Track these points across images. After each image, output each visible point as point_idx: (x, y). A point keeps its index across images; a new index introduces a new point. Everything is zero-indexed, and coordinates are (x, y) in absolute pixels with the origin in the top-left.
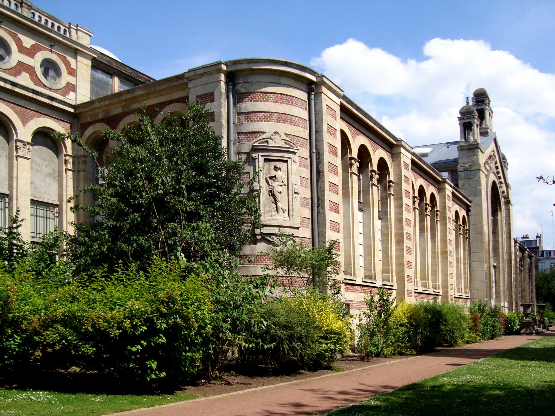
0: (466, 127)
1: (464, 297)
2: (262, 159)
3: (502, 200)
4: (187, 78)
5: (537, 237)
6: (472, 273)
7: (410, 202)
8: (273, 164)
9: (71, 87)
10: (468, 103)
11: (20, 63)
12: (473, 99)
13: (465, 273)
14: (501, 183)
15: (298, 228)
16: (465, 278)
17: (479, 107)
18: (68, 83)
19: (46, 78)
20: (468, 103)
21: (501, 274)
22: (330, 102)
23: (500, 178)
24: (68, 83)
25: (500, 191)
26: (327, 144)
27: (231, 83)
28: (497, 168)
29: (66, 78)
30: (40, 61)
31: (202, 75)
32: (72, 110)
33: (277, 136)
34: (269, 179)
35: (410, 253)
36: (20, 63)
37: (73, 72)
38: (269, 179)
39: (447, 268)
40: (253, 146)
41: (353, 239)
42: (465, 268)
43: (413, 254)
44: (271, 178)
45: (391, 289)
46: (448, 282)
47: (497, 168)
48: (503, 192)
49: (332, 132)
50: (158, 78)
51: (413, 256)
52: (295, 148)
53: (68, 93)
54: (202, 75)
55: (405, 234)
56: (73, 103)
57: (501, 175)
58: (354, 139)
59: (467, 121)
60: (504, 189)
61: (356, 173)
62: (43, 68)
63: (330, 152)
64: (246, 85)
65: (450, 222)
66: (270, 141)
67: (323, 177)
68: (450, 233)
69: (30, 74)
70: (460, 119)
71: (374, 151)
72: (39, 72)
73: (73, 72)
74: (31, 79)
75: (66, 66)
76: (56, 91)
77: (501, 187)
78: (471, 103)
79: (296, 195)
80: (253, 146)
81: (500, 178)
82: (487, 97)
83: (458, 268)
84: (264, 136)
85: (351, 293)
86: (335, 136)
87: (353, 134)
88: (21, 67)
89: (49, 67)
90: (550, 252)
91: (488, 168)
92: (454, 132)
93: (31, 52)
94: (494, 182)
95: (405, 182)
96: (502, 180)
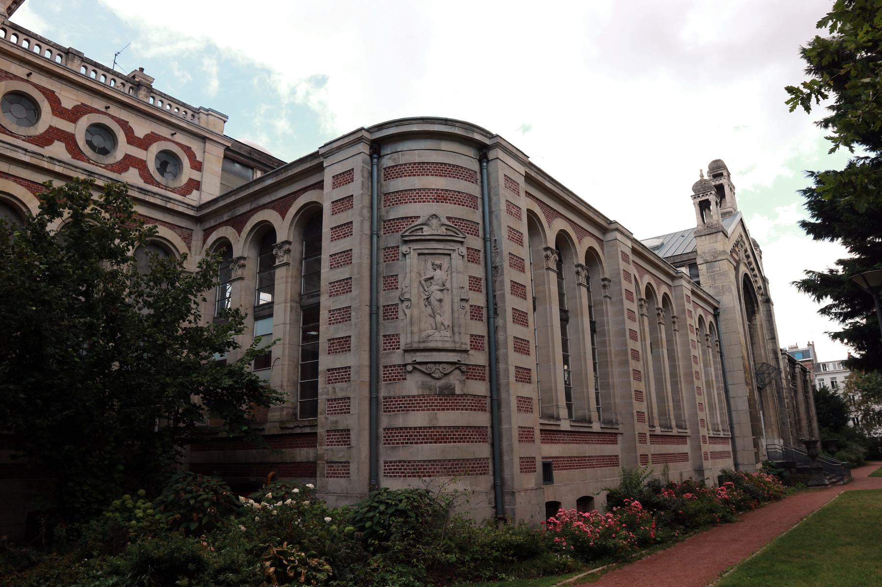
0: (704, 206)
1: (722, 436)
2: (414, 254)
3: (759, 298)
4: (322, 155)
5: (809, 345)
6: (732, 401)
7: (634, 307)
8: (430, 259)
9: (195, 185)
10: (702, 176)
11: (127, 157)
12: (708, 172)
13: (720, 401)
14: (755, 276)
15: (466, 351)
16: (721, 409)
17: (717, 183)
18: (190, 180)
19: (163, 175)
20: (702, 176)
21: (770, 399)
22: (502, 168)
23: (753, 270)
24: (190, 180)
25: (755, 286)
26: (507, 228)
27: (375, 156)
28: (748, 257)
29: (188, 173)
30: (156, 153)
31: (340, 148)
32: (192, 213)
33: (434, 221)
34: (423, 282)
35: (639, 379)
36: (127, 157)
37: (198, 166)
38: (423, 282)
39: (698, 429)
40: (403, 236)
41: (554, 363)
42: (719, 394)
43: (643, 379)
44: (427, 280)
45: (616, 434)
46: (699, 433)
47: (748, 257)
48: (760, 288)
49: (514, 211)
50: (289, 160)
51: (643, 382)
52: (461, 235)
53: (190, 192)
54: (340, 148)
55: (629, 352)
56: (194, 204)
57: (754, 265)
58: (549, 223)
59: (704, 198)
60: (760, 283)
61: (555, 268)
62: (159, 162)
63: (511, 239)
64: (395, 155)
65: (692, 332)
66: (425, 228)
67: (502, 274)
68: (694, 347)
69: (140, 170)
70: (694, 197)
71: (580, 240)
72: (152, 166)
73: (198, 166)
74: (141, 176)
75: (189, 159)
76: (173, 190)
77: (756, 281)
78: (706, 177)
79: (464, 304)
80: (403, 236)
81: (753, 270)
82: (725, 168)
83: (709, 395)
84: (419, 221)
85: (553, 445)
86: (520, 218)
87: (547, 217)
88: (129, 161)
89: (168, 161)
90: (824, 365)
91: (737, 258)
92: (689, 219)
93: (145, 143)
94: (746, 275)
95: (625, 279)
96: (756, 272)
